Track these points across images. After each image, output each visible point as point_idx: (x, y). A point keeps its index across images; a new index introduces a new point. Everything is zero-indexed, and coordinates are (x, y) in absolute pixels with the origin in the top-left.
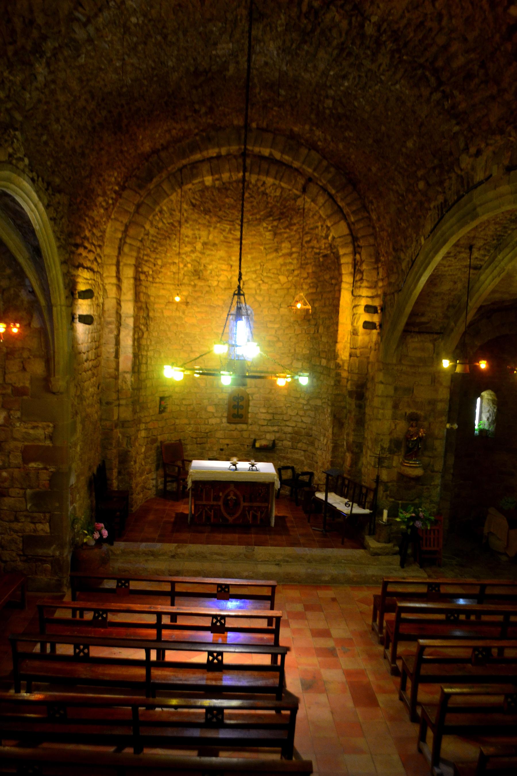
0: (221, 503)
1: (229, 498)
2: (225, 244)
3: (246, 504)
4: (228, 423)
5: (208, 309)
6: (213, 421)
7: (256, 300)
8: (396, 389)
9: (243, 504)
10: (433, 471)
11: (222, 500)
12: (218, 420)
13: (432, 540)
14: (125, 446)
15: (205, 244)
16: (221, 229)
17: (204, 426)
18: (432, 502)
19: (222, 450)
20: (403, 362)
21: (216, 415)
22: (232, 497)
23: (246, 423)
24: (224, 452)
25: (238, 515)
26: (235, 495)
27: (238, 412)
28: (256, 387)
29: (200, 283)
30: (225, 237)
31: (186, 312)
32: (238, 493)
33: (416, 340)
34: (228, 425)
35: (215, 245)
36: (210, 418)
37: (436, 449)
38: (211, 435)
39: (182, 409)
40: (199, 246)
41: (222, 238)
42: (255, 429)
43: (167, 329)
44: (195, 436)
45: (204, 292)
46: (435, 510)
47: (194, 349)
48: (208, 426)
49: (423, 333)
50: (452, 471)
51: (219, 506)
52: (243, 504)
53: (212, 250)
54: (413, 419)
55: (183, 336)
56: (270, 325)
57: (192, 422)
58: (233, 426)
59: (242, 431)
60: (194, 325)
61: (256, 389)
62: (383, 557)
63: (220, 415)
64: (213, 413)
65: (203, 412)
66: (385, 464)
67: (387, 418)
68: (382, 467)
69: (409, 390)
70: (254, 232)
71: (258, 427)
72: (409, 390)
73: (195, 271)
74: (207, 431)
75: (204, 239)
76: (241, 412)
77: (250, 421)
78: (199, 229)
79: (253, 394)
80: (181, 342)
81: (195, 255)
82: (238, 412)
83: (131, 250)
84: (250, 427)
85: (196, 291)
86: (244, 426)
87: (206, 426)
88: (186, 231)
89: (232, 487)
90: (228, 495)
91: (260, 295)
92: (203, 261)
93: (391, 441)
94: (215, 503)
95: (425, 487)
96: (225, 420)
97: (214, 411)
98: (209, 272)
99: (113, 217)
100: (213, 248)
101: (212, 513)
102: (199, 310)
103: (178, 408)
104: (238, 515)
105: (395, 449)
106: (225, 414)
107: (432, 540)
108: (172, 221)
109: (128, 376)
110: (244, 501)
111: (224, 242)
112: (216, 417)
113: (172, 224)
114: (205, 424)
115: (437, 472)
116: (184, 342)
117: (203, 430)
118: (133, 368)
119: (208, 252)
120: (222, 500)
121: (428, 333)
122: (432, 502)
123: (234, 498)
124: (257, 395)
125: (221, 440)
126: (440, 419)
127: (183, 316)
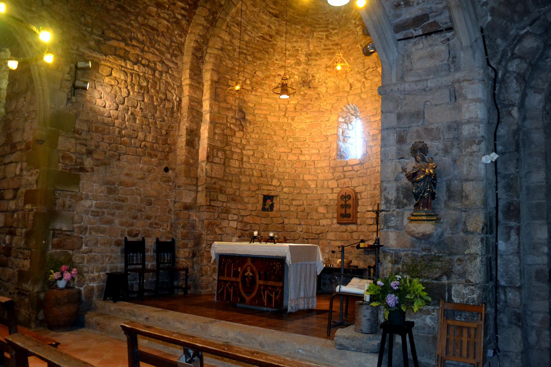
0: (239, 280)
1: (246, 274)
2: (326, 51)
3: (261, 282)
4: (338, 223)
5: (317, 114)
6: (323, 222)
7: (361, 98)
8: (399, 117)
9: (259, 282)
10: (466, 232)
11: (240, 276)
12: (329, 222)
13: (465, 345)
14: (200, 229)
15: (308, 55)
16: (319, 38)
17: (315, 227)
18: (468, 283)
19: (333, 252)
20: (406, 79)
21: (326, 216)
22: (249, 273)
23: (356, 223)
24: (335, 254)
25: (254, 294)
26: (252, 271)
27: (345, 212)
28: (363, 184)
29: (310, 92)
30: (325, 45)
31: (296, 119)
32: (255, 269)
33: (421, 46)
34: (338, 225)
35: (318, 54)
36: (321, 219)
37: (467, 197)
38: (323, 236)
39: (292, 209)
40: (303, 58)
41: (323, 47)
42: (364, 230)
43: (273, 133)
44: (305, 237)
45: (314, 99)
46: (475, 296)
47: (304, 152)
48: (320, 227)
49: (430, 34)
50: (546, 250)
51: (238, 283)
52: (259, 282)
53: (316, 60)
54: (420, 151)
55: (291, 140)
56: (373, 119)
57: (303, 223)
58: (343, 227)
59: (353, 232)
60: (303, 130)
61: (364, 187)
62: (353, 354)
63: (331, 216)
64: (324, 214)
65: (314, 213)
66: (392, 224)
67: (390, 157)
68: (388, 227)
69: (418, 115)
70: (347, 32)
71: (366, 227)
72: (418, 115)
73: (304, 82)
74: (318, 232)
75: (305, 50)
76: (349, 211)
77: (359, 221)
78: (296, 42)
79: (361, 193)
80: (290, 146)
81: (302, 67)
82: (345, 212)
83: (210, 57)
84: (360, 228)
85: (305, 100)
86: (354, 227)
87: (317, 227)
88: (280, 42)
89: (249, 262)
90: (245, 271)
91: (365, 93)
92: (311, 72)
93: (398, 190)
94: (234, 279)
95: (456, 258)
96: (335, 221)
97: (325, 212)
98: (317, 80)
99: (189, 32)
100: (317, 58)
101: (232, 291)
102: (308, 116)
103: (287, 208)
104: (254, 294)
105: (405, 201)
106: (335, 215)
107: (465, 345)
108: (260, 34)
109: (204, 164)
110: (260, 279)
111: (325, 49)
112: (327, 218)
113: (264, 38)
114: (316, 225)
115: (472, 233)
116: (293, 145)
117: (314, 231)
118: (208, 157)
119: (314, 63)
120: (240, 276)
121: (436, 32)
122: (468, 283)
123: (251, 274)
124: (365, 193)
125: (332, 242)
126: (469, 150)
127: (292, 123)
